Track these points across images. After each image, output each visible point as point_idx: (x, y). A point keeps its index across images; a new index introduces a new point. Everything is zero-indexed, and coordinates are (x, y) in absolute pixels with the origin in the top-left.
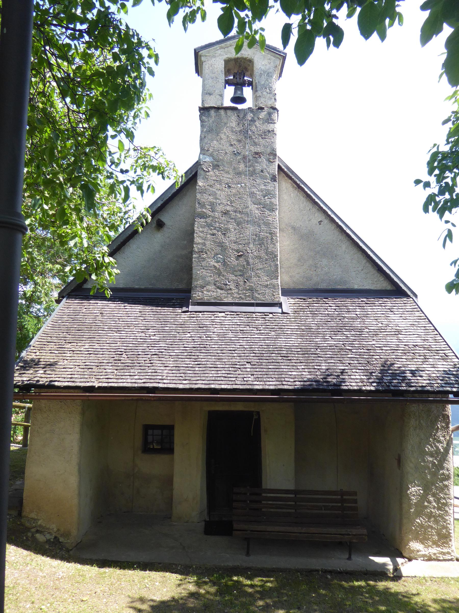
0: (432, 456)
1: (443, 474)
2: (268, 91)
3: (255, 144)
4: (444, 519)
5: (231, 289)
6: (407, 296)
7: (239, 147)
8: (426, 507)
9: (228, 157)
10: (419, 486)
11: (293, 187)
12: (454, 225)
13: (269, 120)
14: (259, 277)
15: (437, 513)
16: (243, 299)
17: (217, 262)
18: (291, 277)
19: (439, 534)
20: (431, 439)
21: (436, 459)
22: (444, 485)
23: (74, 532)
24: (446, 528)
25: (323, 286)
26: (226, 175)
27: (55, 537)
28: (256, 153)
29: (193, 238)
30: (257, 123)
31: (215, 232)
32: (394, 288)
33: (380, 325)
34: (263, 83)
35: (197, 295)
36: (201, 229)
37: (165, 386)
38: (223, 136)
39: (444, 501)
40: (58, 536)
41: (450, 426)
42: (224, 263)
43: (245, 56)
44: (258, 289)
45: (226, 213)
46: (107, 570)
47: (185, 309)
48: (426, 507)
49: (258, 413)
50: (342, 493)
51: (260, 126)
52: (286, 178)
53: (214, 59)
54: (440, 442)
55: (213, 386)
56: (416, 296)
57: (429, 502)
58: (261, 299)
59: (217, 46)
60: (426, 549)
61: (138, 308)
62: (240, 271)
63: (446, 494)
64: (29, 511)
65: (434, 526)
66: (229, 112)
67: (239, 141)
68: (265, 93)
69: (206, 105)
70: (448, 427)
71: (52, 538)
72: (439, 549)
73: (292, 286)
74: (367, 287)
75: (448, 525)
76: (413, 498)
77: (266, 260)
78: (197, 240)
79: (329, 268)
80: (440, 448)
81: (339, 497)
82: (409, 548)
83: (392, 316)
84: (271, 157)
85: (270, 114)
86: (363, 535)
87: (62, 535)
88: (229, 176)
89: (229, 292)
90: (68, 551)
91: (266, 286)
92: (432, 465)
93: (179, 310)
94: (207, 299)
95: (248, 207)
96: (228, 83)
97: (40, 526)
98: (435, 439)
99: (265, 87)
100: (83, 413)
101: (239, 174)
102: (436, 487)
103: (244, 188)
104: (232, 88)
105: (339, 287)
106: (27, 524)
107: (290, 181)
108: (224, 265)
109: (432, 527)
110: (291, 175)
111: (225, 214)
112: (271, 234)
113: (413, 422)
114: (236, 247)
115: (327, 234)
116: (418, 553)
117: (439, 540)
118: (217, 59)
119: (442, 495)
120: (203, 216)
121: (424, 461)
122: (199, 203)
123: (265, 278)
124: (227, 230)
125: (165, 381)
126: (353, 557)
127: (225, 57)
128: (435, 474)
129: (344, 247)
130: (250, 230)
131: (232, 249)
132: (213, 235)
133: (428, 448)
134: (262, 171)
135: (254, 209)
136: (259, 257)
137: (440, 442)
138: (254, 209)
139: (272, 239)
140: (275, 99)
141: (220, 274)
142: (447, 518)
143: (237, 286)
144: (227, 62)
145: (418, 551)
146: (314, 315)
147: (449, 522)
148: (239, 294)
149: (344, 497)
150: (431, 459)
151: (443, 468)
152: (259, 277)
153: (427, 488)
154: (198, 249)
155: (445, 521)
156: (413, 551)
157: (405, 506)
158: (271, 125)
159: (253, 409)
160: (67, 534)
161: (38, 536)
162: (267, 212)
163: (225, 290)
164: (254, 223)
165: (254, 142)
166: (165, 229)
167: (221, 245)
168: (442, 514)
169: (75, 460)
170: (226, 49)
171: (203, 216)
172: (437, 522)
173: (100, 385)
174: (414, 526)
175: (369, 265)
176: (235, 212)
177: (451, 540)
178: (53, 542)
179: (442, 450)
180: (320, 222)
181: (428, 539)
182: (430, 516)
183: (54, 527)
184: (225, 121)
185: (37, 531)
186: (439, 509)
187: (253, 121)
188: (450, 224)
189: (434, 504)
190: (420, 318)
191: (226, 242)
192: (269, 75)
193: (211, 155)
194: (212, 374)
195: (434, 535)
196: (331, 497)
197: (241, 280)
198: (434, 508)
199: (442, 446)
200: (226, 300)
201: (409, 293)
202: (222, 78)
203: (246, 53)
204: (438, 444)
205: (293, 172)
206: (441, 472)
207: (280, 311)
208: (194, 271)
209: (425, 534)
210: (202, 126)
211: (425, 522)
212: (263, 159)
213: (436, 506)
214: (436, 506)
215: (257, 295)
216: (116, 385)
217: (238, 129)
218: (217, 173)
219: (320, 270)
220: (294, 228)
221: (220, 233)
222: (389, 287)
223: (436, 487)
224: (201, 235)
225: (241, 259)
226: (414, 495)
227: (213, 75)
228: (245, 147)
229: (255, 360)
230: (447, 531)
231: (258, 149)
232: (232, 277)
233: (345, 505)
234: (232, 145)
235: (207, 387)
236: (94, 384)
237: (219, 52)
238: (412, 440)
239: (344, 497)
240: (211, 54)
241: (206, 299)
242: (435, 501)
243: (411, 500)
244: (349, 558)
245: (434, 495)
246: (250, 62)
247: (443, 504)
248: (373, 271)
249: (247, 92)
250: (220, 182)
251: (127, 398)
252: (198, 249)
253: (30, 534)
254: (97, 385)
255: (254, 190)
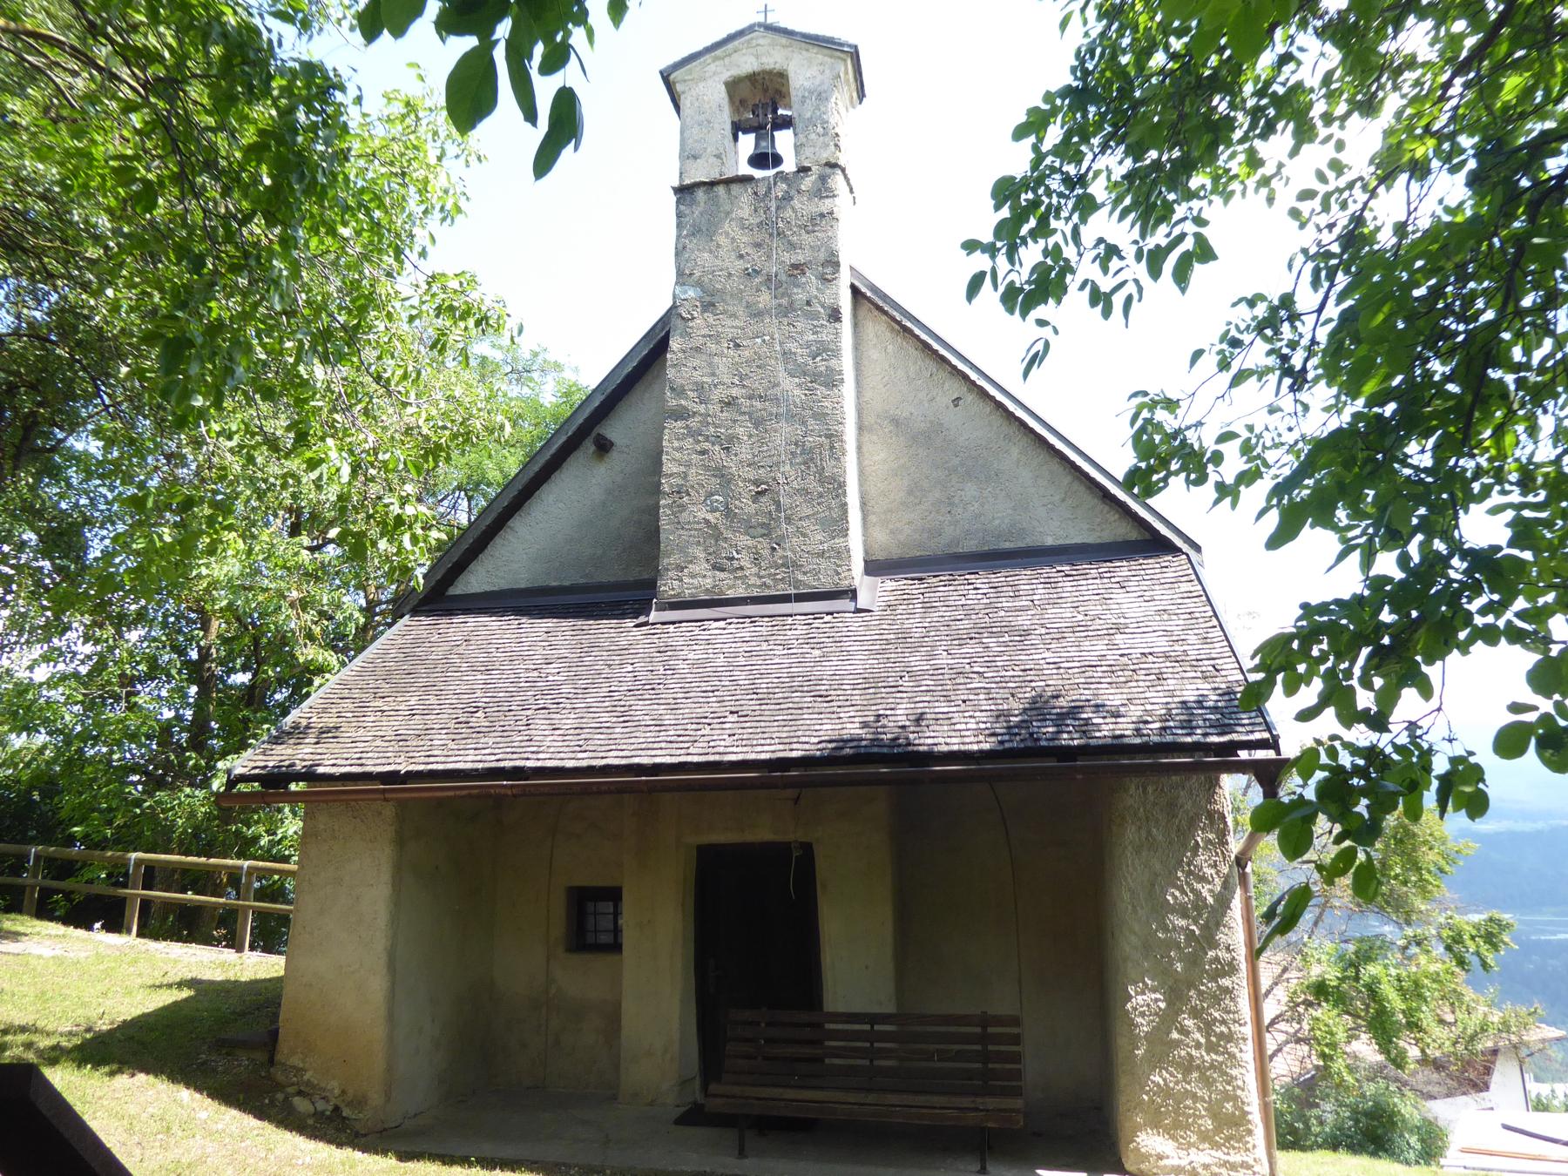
0: (1185, 916)
1: (1217, 959)
2: (819, 130)
3: (792, 246)
4: (1226, 1074)
5: (742, 568)
6: (1173, 550)
7: (757, 257)
8: (1177, 1044)
9: (735, 284)
10: (1154, 990)
11: (893, 329)
12: (1056, 332)
13: (823, 190)
14: (804, 535)
15: (1207, 1058)
16: (769, 587)
17: (713, 510)
18: (892, 532)
19: (1215, 1113)
20: (1180, 874)
21: (1196, 923)
22: (1219, 987)
23: (376, 1098)
24: (1235, 1098)
25: (970, 546)
26: (729, 322)
27: (337, 1109)
28: (795, 266)
29: (661, 464)
30: (796, 203)
31: (707, 445)
32: (1147, 536)
33: (1080, 617)
34: (808, 115)
35: (669, 586)
36: (676, 444)
37: (539, 764)
38: (722, 240)
39: (1224, 1029)
40: (342, 1106)
41: (1230, 839)
42: (728, 513)
43: (768, 68)
44: (803, 562)
45: (730, 403)
46: (410, 1165)
47: (642, 619)
48: (1177, 1044)
49: (807, 848)
50: (985, 1021)
51: (803, 206)
52: (876, 313)
53: (701, 85)
54: (1203, 879)
55: (636, 760)
56: (1197, 548)
57: (1184, 1032)
58: (811, 583)
59: (708, 57)
60: (1183, 1153)
61: (549, 623)
62: (763, 525)
63: (1229, 1012)
64: (287, 1052)
65: (1200, 1093)
66: (735, 188)
67: (758, 245)
68: (813, 136)
69: (687, 182)
70: (1223, 843)
71: (328, 1108)
72: (1219, 1154)
73: (896, 553)
74: (1078, 540)
75: (1239, 1092)
76: (1139, 1020)
77: (821, 496)
78: (669, 467)
79: (982, 505)
80: (1205, 893)
81: (978, 1030)
82: (1137, 1149)
83: (1120, 596)
84: (829, 270)
85: (823, 179)
86: (1012, 1110)
87: (349, 1104)
88: (737, 323)
89: (740, 574)
90: (357, 1135)
91: (822, 554)
92: (1187, 936)
93: (630, 623)
94: (692, 595)
95: (778, 385)
96: (738, 128)
97: (308, 1083)
98: (1190, 873)
99: (811, 122)
100: (400, 841)
101: (759, 315)
102: (1200, 993)
103: (770, 345)
104: (752, 137)
105: (1007, 545)
106: (280, 1077)
107: (884, 318)
108: (727, 517)
109: (1194, 1097)
110: (881, 303)
111: (729, 404)
112: (827, 436)
113: (1131, 833)
114: (751, 474)
115: (970, 426)
116: (1161, 1163)
117: (1218, 1130)
118: (710, 82)
119: (1216, 1015)
120: (681, 414)
121: (1166, 929)
122: (672, 389)
123: (819, 537)
124: (732, 439)
125: (541, 756)
126: (989, 1168)
127: (727, 75)
128: (1194, 961)
129: (1015, 451)
130: (783, 434)
131: (745, 480)
132: (703, 452)
133: (1172, 896)
134: (808, 303)
135: (790, 386)
136: (805, 492)
137: (1203, 879)
138: (790, 386)
139: (832, 447)
140: (836, 145)
141: (718, 536)
142: (1234, 1072)
143: (756, 560)
144: (733, 86)
145: (1160, 1157)
146: (928, 607)
147: (1240, 1083)
148: (761, 577)
149: (991, 1030)
150: (1182, 923)
151: (1215, 945)
152: (804, 535)
153: (1176, 995)
154: (671, 486)
155: (1230, 1080)
156: (1146, 1157)
157: (1122, 1042)
158: (827, 201)
159: (790, 837)
160: (359, 1103)
161: (297, 1101)
162: (821, 391)
163: (730, 572)
164: (791, 417)
165: (790, 243)
166: (614, 454)
167: (720, 473)
168: (1221, 1063)
169: (380, 943)
170: (727, 60)
171: (681, 414)
172: (1208, 1083)
173: (410, 768)
174: (1147, 1093)
175: (1078, 487)
176: (750, 398)
177: (1250, 1132)
178: (328, 1118)
179: (1210, 900)
180: (956, 402)
181: (1187, 1127)
182: (1188, 1066)
183: (334, 1086)
184: (727, 208)
185: (300, 1093)
186: (1211, 1048)
187: (787, 198)
188: (1049, 328)
189: (1197, 1036)
190: (1189, 595)
191: (732, 465)
192: (822, 97)
193: (699, 284)
194: (642, 737)
195: (1202, 1117)
196: (952, 1029)
197: (763, 546)
198: (1198, 1046)
199: (1211, 891)
200: (731, 594)
201: (1178, 542)
202: (725, 119)
203: (771, 61)
204: (1199, 886)
205: (885, 297)
206: (1211, 954)
207: (851, 606)
208: (663, 536)
209: (1177, 1111)
210: (679, 226)
211: (1177, 1083)
212: (811, 278)
213: (1203, 1040)
214: (1203, 1040)
215: (800, 577)
216: (441, 767)
217: (754, 221)
218: (711, 320)
219: (960, 510)
220: (896, 422)
221: (717, 448)
222: (1134, 535)
223: (1200, 993)
224: (678, 455)
225: (763, 499)
226: (1143, 1014)
227: (702, 117)
228: (769, 257)
229: (749, 706)
230: (1235, 1107)
231: (800, 257)
232: (744, 540)
233: (990, 1048)
234: (741, 257)
235: (624, 762)
236: (398, 768)
237: (712, 67)
238: (1130, 875)
239: (991, 1030)
240: (695, 75)
241: (688, 594)
242: (1199, 1029)
243: (1137, 1026)
244: (983, 1170)
245: (1196, 1013)
246: (782, 76)
247: (1221, 1036)
248: (1091, 501)
249: (784, 141)
250: (716, 338)
251: (451, 793)
252: (671, 486)
253: (280, 1096)
254: (403, 768)
255: (792, 346)
